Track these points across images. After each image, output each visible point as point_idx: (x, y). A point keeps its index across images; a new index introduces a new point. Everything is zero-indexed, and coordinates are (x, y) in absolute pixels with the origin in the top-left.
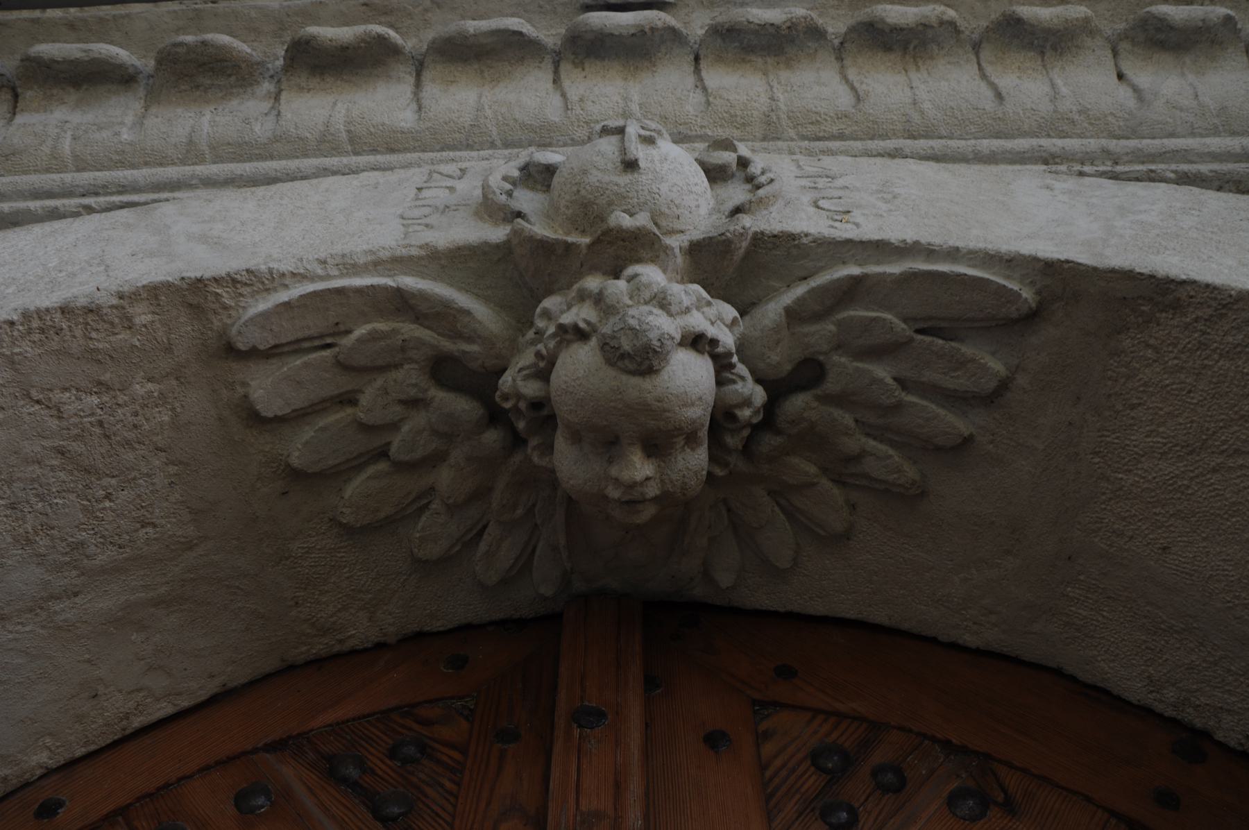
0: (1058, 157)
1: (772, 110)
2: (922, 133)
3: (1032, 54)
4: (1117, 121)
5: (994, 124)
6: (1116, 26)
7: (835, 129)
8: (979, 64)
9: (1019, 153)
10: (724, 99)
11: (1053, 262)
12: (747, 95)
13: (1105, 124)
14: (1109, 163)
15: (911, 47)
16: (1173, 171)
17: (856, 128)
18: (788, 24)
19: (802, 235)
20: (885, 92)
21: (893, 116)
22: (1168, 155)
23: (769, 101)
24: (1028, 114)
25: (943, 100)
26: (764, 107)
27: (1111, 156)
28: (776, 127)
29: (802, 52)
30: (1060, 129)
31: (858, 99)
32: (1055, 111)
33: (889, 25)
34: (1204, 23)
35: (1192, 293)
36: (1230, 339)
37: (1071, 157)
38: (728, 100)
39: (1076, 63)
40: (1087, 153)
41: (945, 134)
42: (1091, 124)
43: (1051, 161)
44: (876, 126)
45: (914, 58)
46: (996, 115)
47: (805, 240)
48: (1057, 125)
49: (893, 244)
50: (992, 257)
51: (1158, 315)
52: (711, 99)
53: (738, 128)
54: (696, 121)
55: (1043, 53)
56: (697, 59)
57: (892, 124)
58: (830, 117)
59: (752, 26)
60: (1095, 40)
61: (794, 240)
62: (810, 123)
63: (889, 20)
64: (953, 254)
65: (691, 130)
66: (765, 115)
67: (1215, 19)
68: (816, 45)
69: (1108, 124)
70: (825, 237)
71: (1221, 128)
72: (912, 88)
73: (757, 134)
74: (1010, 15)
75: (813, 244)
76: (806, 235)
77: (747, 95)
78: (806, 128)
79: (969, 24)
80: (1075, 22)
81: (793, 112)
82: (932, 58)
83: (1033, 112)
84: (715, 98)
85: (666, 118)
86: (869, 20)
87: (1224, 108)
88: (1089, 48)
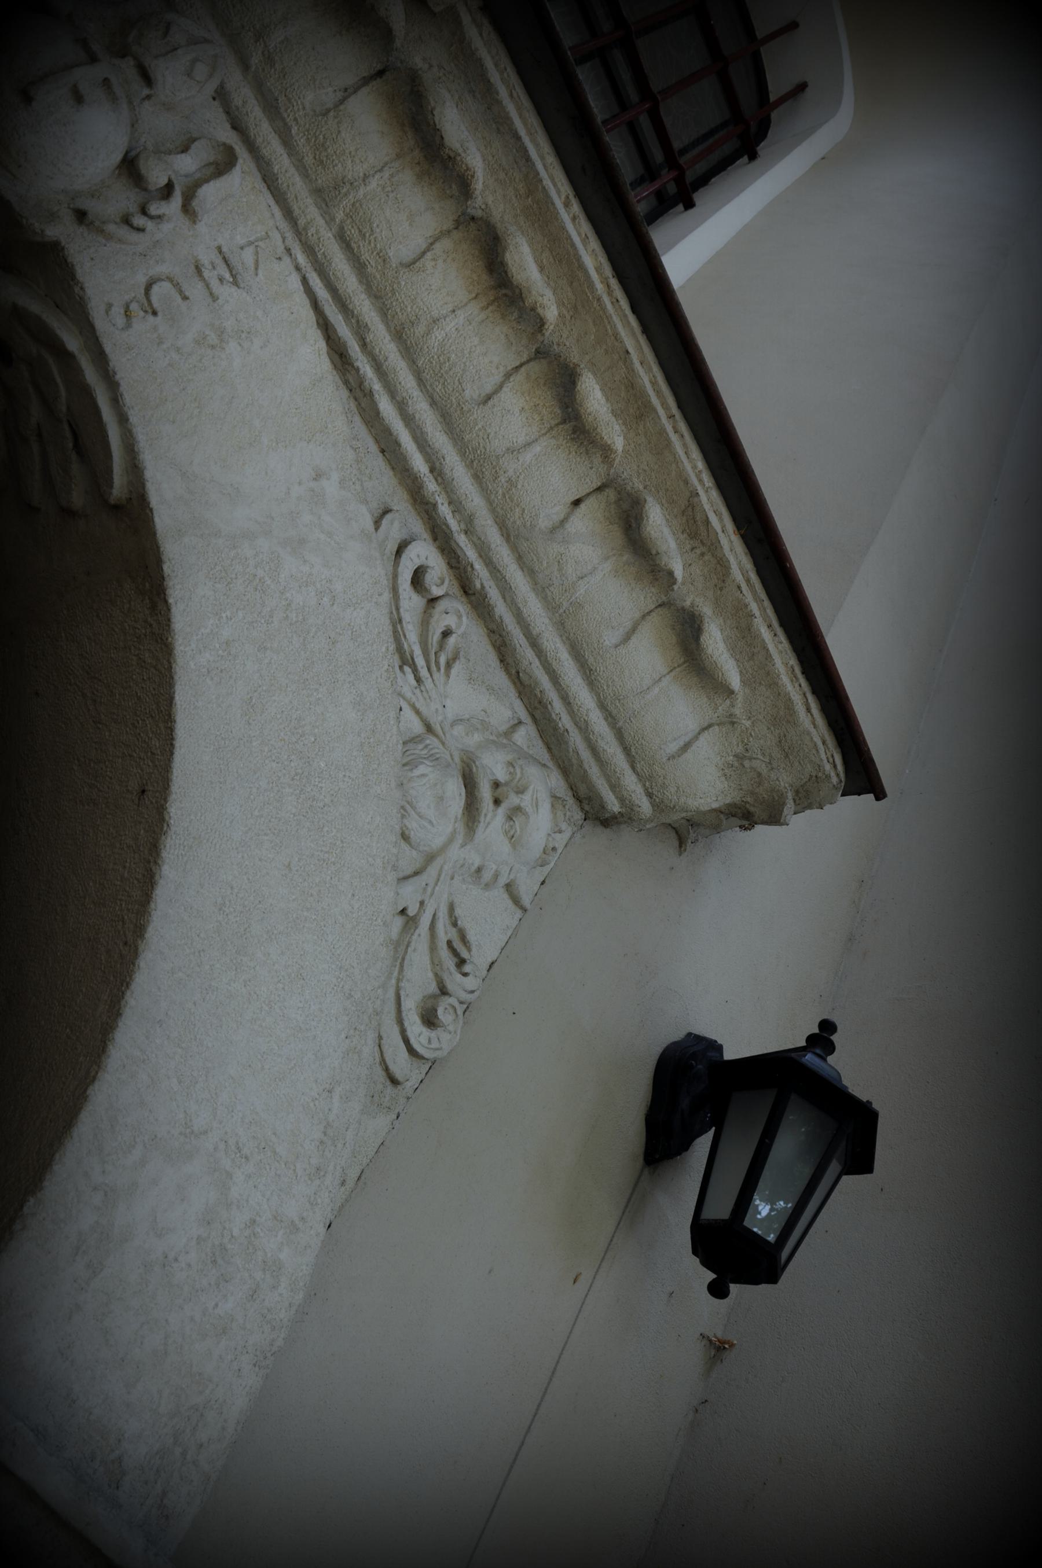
0: (442, 478)
1: (351, 184)
2: (409, 342)
3: (559, 412)
4: (519, 518)
5: (455, 406)
6: (635, 480)
7: (365, 256)
8: (521, 365)
9: (426, 441)
10: (339, 127)
11: (145, 500)
12: (357, 150)
13: (510, 508)
14: (463, 526)
15: (504, 291)
16: (482, 584)
17: (378, 276)
18: (452, 155)
19: (80, 285)
20: (433, 287)
21: (409, 307)
22: (498, 574)
23: (361, 175)
24: (481, 434)
25: (453, 347)
26: (351, 173)
27: (469, 525)
28: (336, 197)
29: (443, 183)
30: (484, 470)
31: (410, 265)
32: (497, 457)
33: (504, 258)
34: (656, 555)
35: (162, 612)
36: (147, 655)
37: (449, 490)
38: (339, 132)
39: (571, 456)
40: (461, 503)
41: (419, 365)
42: (504, 495)
43: (435, 474)
44: (390, 295)
45: (496, 299)
46: (464, 404)
47: (77, 289)
48: (486, 464)
49: (109, 365)
50: (133, 450)
51: (147, 597)
52: (332, 114)
53: (315, 158)
54: (298, 109)
55: (564, 422)
56: (380, 73)
57: (401, 310)
58: (376, 245)
59: (430, 117)
60: (602, 466)
61: (72, 280)
62: (359, 228)
63: (508, 255)
64: (123, 419)
65: (286, 110)
66: (343, 180)
67: (663, 563)
68: (457, 194)
69: (511, 510)
70: (87, 305)
71: (561, 611)
72: (454, 311)
73: (320, 181)
74: (576, 372)
75: (78, 298)
76: (82, 288)
77: (357, 150)
78: (353, 227)
79: (568, 338)
80: (598, 437)
81: (361, 205)
82: (503, 317)
83: (485, 437)
84: (335, 117)
85: (284, 76)
86: (500, 235)
87: (581, 606)
88: (592, 462)
